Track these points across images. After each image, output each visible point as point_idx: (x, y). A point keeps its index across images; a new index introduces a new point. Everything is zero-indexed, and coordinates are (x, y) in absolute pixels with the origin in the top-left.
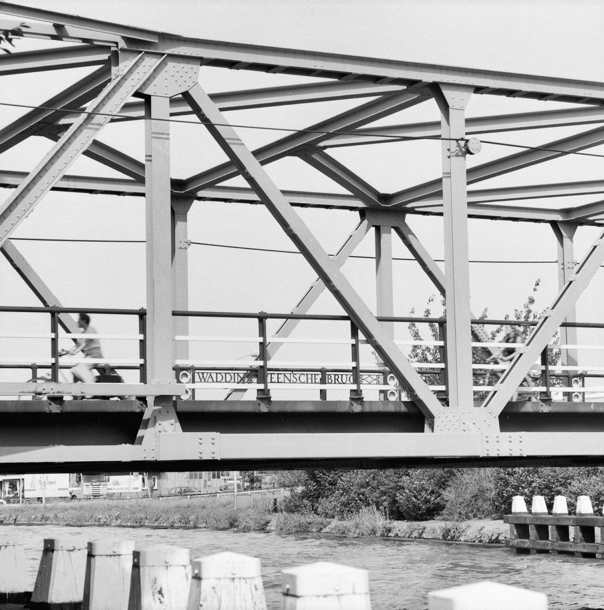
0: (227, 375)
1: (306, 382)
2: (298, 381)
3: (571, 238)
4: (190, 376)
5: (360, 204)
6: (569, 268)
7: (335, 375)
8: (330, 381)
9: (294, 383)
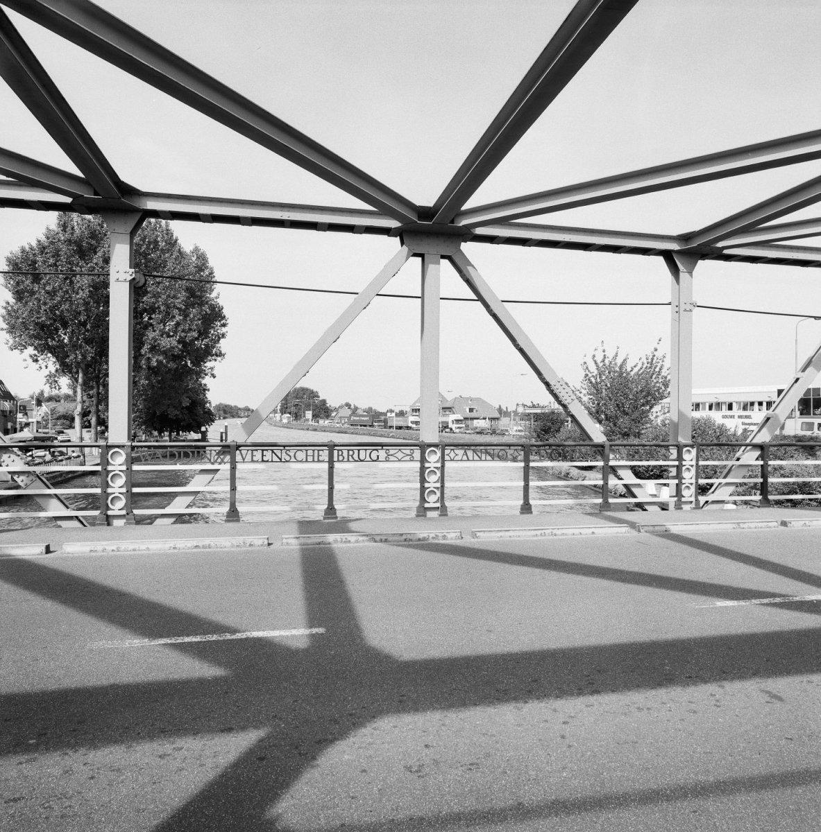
0: (361, 451)
1: (304, 460)
2: (293, 459)
3: (690, 273)
4: (439, 454)
5: (393, 224)
6: (685, 310)
7: (348, 450)
8: (341, 458)
9: (287, 461)
